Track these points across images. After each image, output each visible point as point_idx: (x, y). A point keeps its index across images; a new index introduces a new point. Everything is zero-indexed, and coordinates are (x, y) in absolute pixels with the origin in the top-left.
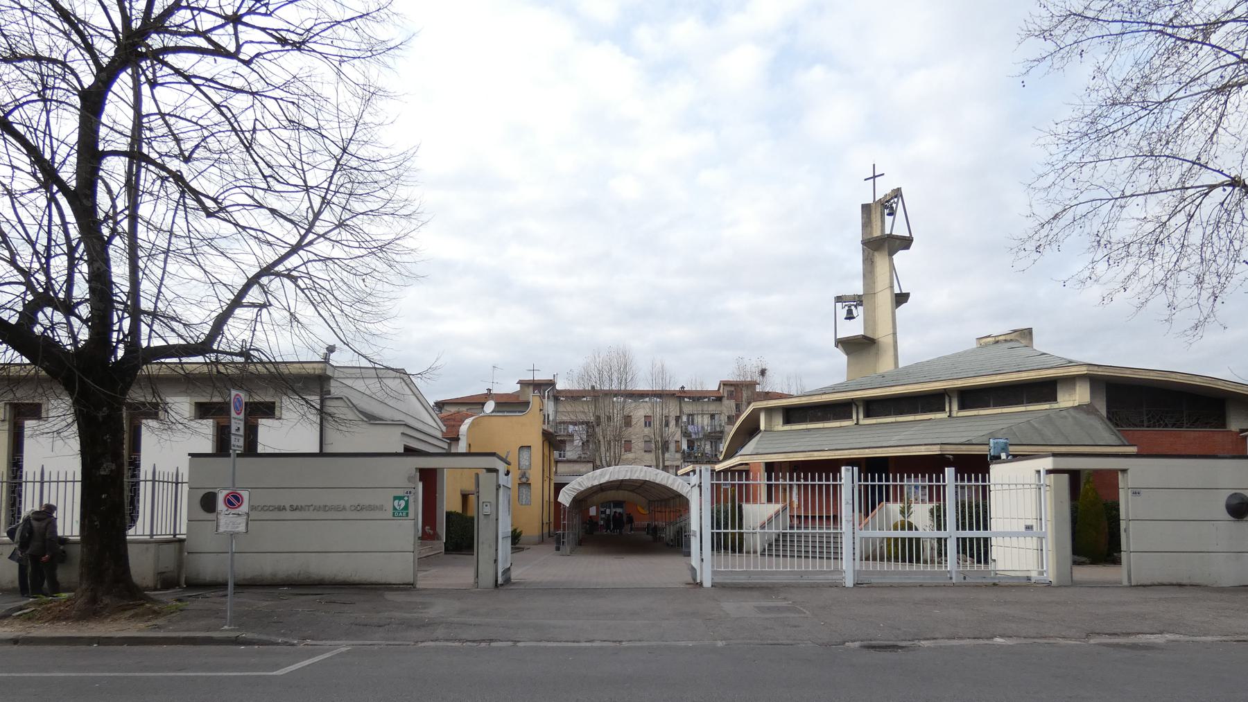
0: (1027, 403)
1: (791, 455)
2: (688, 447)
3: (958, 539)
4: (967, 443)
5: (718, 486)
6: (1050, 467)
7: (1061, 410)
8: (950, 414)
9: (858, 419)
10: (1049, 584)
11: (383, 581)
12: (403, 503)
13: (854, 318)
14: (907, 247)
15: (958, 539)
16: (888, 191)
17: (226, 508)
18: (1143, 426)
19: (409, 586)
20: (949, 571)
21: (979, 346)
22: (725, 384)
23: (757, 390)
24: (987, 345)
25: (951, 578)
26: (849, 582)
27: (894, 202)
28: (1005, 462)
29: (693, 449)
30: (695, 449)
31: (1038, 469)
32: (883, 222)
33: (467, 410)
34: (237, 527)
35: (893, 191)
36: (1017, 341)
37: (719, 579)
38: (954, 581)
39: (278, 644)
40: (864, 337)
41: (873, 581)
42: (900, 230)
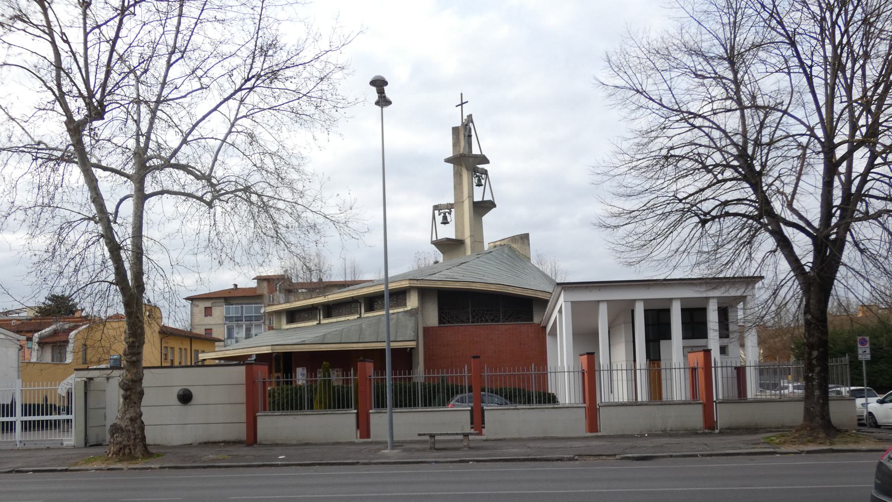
3: (22, 422)
18: (469, 322)
33: (212, 304)
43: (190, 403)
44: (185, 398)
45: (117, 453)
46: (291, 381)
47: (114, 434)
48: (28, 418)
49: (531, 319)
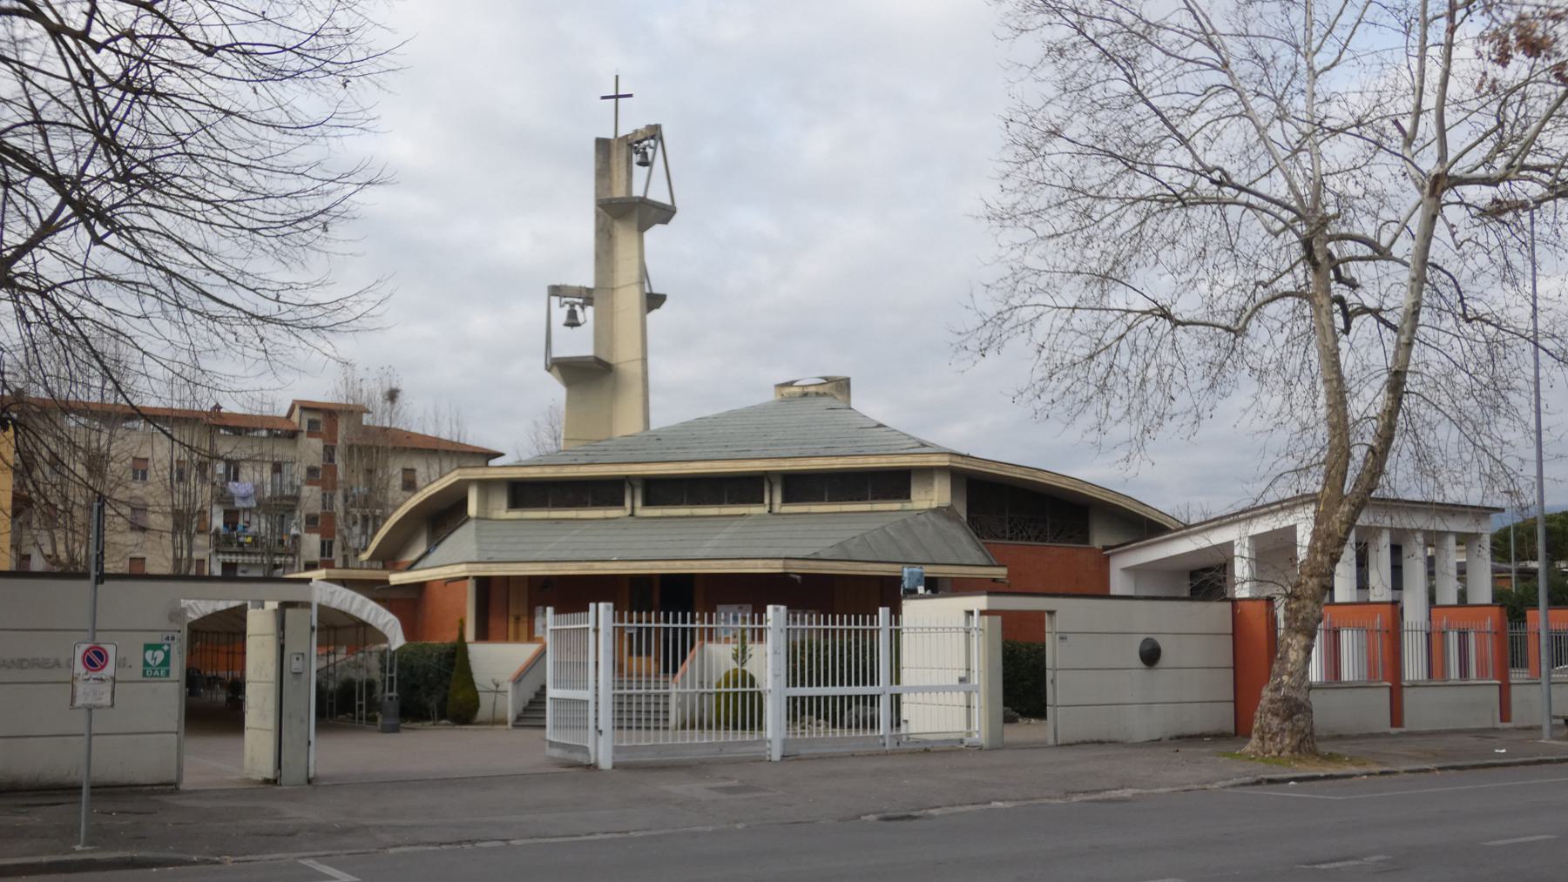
0: (873, 499)
1: (557, 566)
2: (226, 524)
4: (813, 557)
5: (622, 629)
6: (984, 607)
7: (920, 512)
8: (771, 508)
9: (633, 508)
10: (981, 748)
11: (126, 780)
12: (160, 655)
13: (578, 325)
14: (666, 221)
15: (892, 695)
16: (641, 126)
17: (85, 671)
18: (1004, 538)
19: (170, 787)
20: (882, 736)
21: (779, 397)
22: (306, 407)
23: (364, 423)
24: (791, 398)
25: (884, 744)
26: (776, 756)
27: (649, 146)
28: (922, 597)
29: (235, 529)
30: (240, 528)
31: (970, 609)
32: (630, 173)
34: (100, 699)
35: (649, 127)
36: (832, 395)
37: (623, 758)
38: (887, 748)
39: (194, 863)
40: (597, 360)
41: (801, 752)
42: (658, 194)
43: (1156, 666)
44: (1151, 655)
45: (1297, 749)
46: (710, 630)
47: (1293, 714)
48: (799, 691)
49: (1086, 540)
